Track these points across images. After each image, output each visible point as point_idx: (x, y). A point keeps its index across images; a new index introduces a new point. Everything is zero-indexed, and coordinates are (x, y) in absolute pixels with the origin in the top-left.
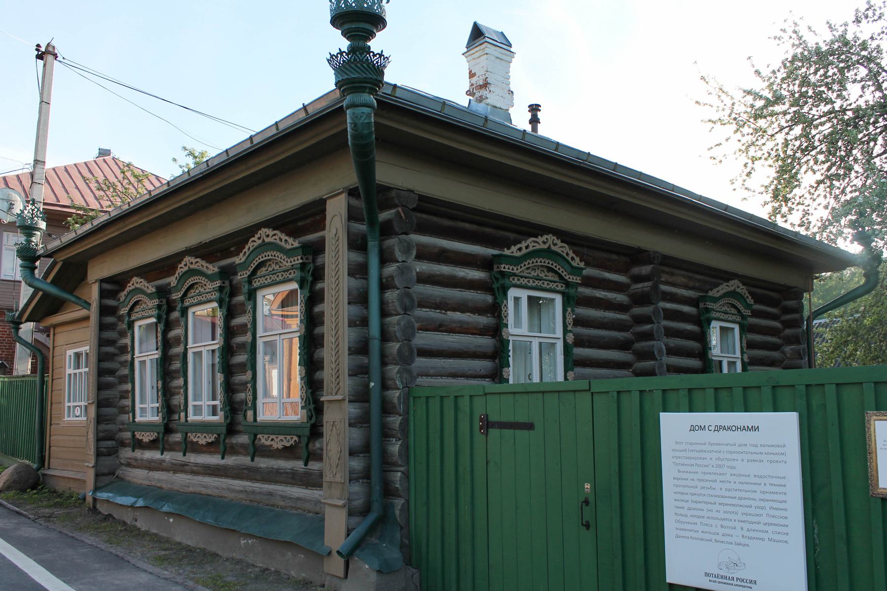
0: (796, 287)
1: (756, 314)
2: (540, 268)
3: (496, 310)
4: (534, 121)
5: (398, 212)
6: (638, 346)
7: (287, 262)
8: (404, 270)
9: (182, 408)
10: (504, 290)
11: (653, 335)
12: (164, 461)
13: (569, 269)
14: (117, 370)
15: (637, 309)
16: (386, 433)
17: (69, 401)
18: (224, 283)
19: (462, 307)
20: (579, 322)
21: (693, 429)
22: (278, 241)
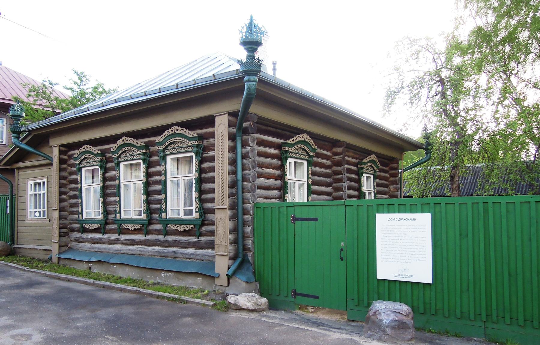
0: (396, 158)
1: (381, 171)
2: (300, 149)
3: (282, 168)
4: (274, 69)
5: (250, 123)
6: (335, 185)
7: (189, 143)
8: (252, 150)
9: (118, 212)
10: (286, 159)
11: (342, 180)
12: (103, 238)
13: (311, 149)
14: (68, 193)
15: (335, 168)
16: (245, 223)
18: (146, 151)
19: (269, 166)
20: (314, 174)
21: (390, 220)
22: (184, 133)
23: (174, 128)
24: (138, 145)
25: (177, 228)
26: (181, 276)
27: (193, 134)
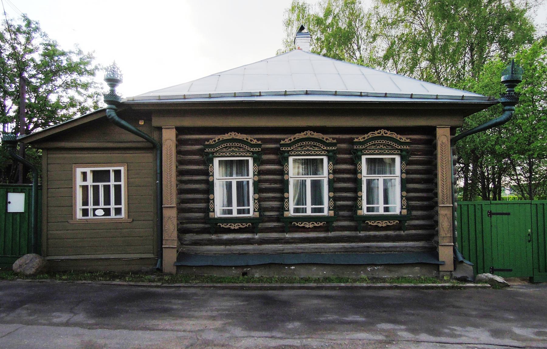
17: (248, 211)
23: (383, 131)
24: (327, 142)
25: (230, 227)
26: (392, 268)
27: (406, 140)
